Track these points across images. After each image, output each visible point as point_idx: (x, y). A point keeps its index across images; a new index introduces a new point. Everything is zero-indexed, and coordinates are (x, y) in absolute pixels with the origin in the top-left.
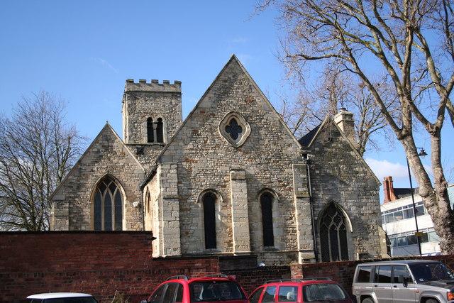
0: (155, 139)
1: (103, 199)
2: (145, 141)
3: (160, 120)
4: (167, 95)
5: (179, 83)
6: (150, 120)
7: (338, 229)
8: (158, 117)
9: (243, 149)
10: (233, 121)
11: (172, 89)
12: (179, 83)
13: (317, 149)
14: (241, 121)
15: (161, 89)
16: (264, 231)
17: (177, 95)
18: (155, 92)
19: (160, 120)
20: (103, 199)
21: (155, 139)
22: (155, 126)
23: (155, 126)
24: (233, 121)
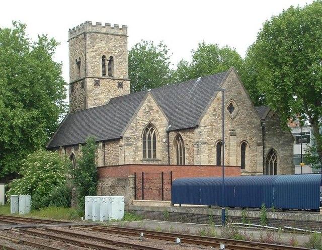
0: (107, 75)
1: (147, 136)
2: (101, 75)
3: (111, 57)
4: (117, 37)
5: (125, 27)
6: (104, 57)
7: (273, 162)
8: (110, 55)
9: (235, 119)
10: (231, 104)
11: (121, 32)
12: (125, 27)
13: (267, 120)
14: (234, 105)
15: (112, 31)
16: (244, 160)
17: (124, 37)
18: (108, 34)
19: (111, 57)
20: (147, 136)
21: (107, 75)
22: (107, 62)
23: (107, 62)
24: (231, 104)
